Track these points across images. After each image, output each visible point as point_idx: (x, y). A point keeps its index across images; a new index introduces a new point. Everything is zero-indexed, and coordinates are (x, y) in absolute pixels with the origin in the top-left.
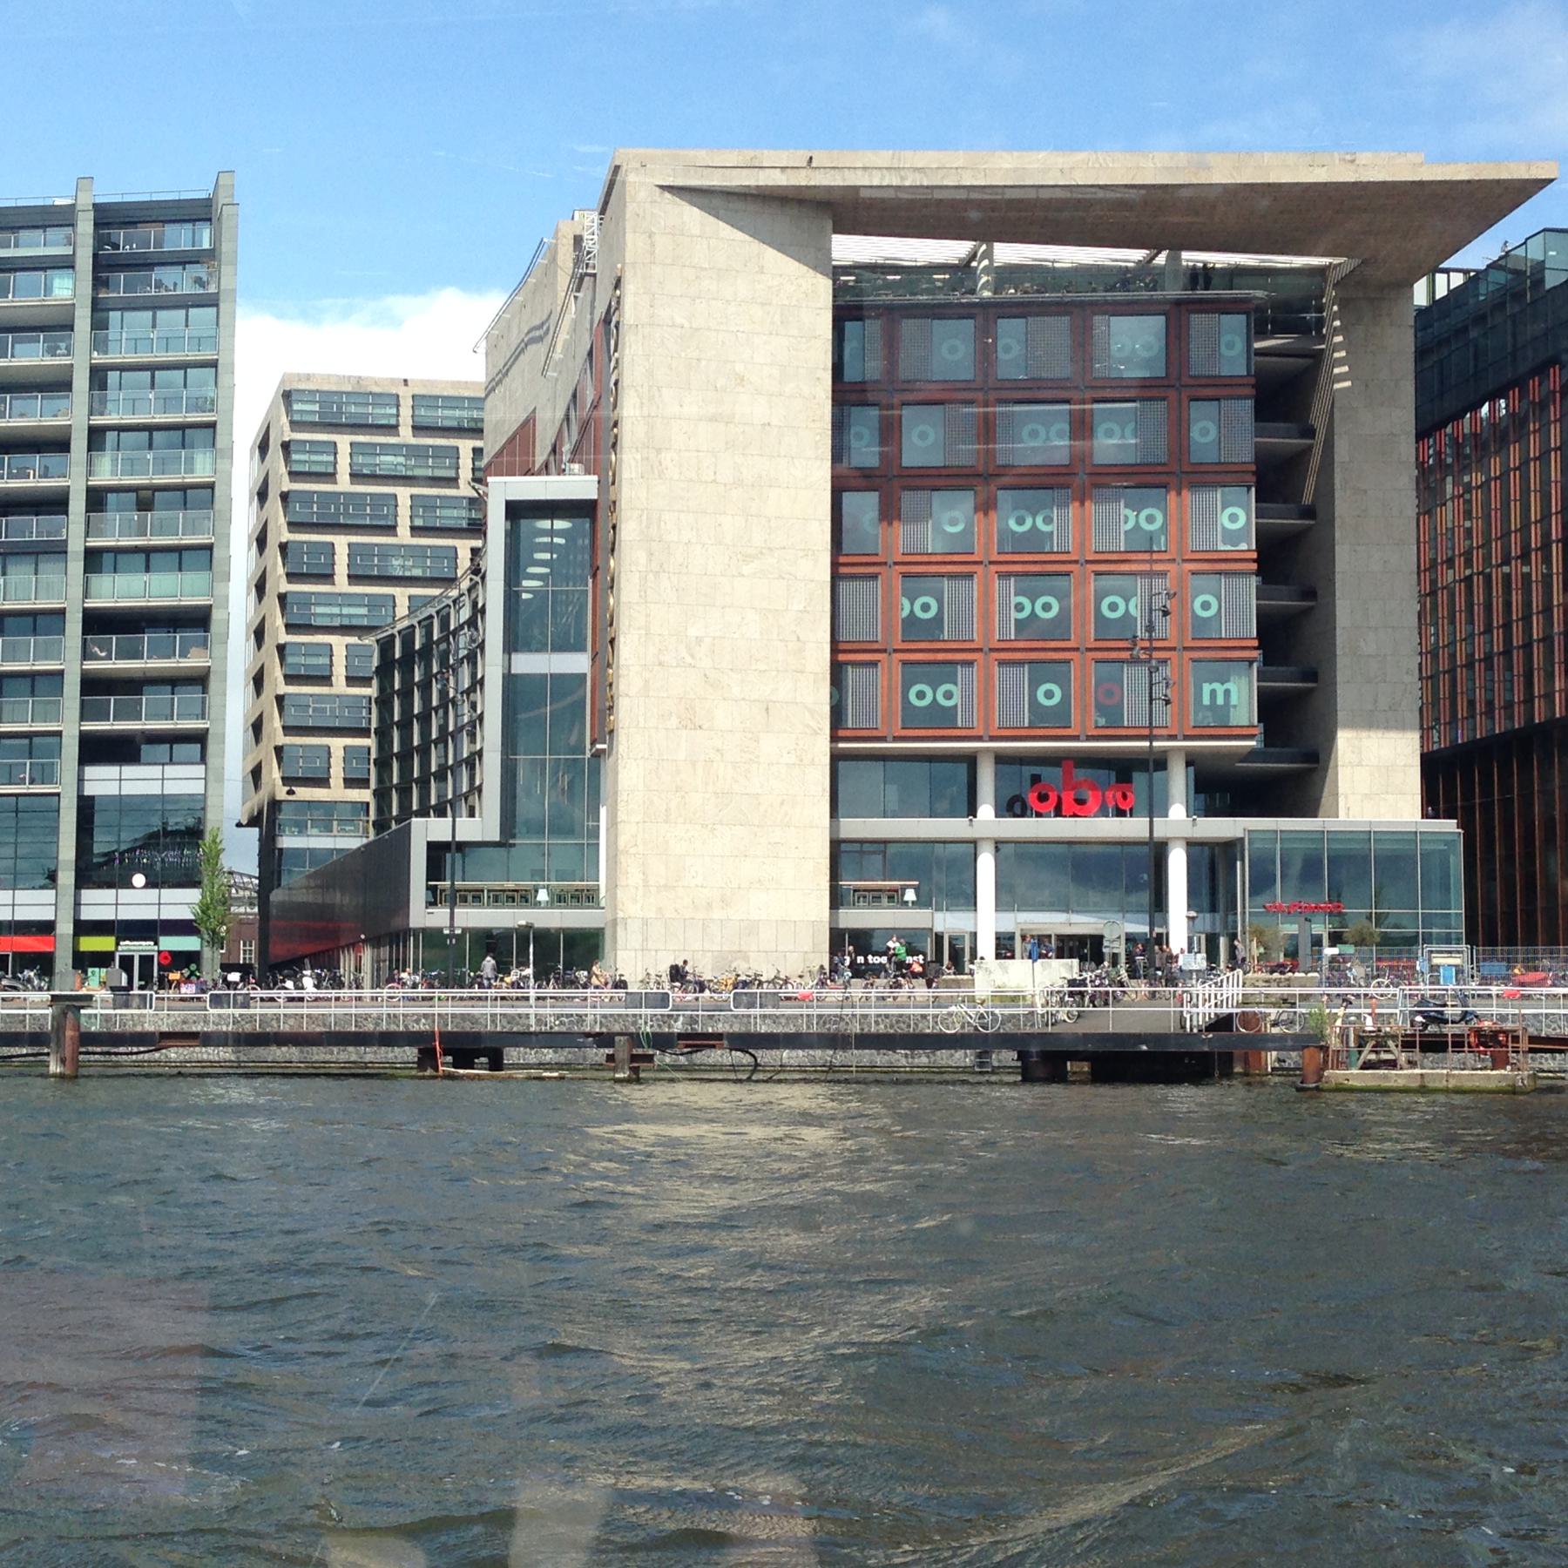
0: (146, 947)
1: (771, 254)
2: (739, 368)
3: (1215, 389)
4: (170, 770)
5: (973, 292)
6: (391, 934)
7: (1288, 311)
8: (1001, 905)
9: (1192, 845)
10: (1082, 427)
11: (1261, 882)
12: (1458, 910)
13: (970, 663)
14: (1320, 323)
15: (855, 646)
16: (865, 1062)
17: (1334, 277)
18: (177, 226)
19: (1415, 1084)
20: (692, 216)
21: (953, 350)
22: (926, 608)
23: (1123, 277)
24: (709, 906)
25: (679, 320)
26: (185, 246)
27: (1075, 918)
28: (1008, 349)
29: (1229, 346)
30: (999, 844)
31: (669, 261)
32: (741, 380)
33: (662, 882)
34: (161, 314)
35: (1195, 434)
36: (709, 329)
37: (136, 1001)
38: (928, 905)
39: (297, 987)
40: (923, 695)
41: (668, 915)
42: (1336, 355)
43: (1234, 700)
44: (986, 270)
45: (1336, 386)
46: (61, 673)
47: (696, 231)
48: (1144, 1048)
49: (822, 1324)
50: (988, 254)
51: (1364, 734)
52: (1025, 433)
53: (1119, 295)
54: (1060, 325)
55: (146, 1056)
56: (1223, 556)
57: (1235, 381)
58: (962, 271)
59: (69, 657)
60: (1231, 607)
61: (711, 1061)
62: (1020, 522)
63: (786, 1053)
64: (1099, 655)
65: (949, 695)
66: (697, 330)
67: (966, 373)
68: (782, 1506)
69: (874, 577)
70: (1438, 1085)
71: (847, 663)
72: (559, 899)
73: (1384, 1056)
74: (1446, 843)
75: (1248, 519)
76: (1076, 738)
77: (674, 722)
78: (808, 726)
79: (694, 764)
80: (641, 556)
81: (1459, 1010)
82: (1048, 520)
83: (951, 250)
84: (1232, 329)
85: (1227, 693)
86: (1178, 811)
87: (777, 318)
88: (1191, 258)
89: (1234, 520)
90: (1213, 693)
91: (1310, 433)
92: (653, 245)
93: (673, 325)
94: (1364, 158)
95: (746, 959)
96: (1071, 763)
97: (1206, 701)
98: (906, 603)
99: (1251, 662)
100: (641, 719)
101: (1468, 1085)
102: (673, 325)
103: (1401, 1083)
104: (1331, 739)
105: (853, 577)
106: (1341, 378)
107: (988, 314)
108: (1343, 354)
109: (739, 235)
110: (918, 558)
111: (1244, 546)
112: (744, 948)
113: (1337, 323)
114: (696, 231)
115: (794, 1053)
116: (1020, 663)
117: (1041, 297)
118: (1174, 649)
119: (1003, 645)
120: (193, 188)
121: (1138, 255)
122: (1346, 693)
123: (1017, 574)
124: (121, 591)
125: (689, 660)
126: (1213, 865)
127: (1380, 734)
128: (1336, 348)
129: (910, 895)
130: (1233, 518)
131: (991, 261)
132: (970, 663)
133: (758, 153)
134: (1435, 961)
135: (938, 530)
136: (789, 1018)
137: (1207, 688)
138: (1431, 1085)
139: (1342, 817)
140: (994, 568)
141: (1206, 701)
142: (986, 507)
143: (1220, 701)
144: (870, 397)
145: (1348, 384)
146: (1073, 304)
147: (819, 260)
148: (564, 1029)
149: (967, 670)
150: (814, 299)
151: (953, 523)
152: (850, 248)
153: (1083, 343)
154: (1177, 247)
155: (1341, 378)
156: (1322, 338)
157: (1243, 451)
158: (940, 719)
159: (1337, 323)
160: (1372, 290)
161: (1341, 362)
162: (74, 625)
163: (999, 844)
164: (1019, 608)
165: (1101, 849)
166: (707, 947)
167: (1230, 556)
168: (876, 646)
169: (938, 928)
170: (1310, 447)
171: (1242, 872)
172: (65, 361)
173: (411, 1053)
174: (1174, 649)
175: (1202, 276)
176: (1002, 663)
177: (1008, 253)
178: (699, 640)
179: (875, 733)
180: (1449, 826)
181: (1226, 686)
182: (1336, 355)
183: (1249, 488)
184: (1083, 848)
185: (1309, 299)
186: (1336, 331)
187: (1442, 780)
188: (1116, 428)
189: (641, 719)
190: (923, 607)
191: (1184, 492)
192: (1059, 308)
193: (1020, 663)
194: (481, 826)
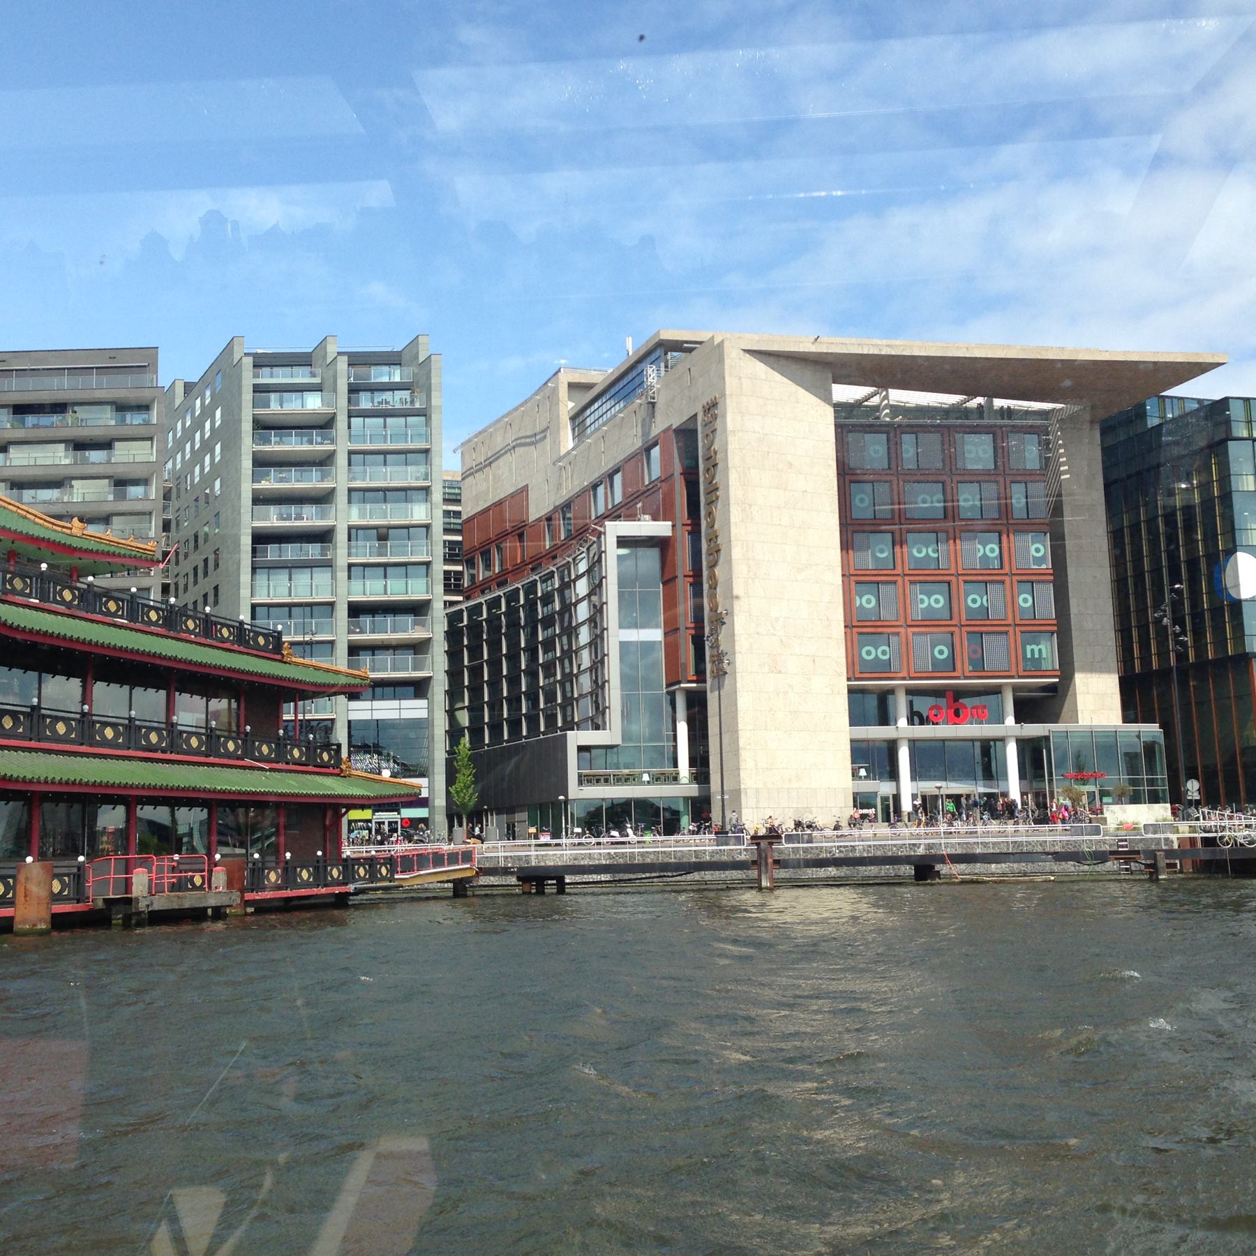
0: (392, 816)
1: (802, 391)
4: (377, 704)
6: (541, 805)
8: (915, 776)
9: (913, 743)
18: (379, 368)
20: (760, 368)
26: (385, 379)
28: (907, 452)
30: (913, 743)
32: (790, 465)
34: (389, 420)
37: (733, 841)
39: (622, 836)
43: (1044, 655)
46: (332, 643)
47: (763, 377)
51: (1089, 675)
52: (919, 499)
54: (934, 439)
55: (679, 878)
59: (341, 631)
62: (919, 551)
63: (993, 866)
64: (969, 629)
72: (656, 779)
85: (1040, 650)
90: (1032, 650)
95: (811, 812)
97: (1029, 656)
99: (1052, 633)
106: (1065, 472)
107: (892, 432)
109: (785, 380)
111: (1044, 566)
114: (763, 377)
117: (918, 421)
120: (397, 344)
124: (372, 590)
128: (1061, 456)
129: (646, 778)
130: (1037, 550)
135: (874, 556)
136: (994, 844)
137: (1029, 648)
139: (1080, 723)
141: (1029, 656)
142: (898, 541)
143: (1037, 656)
147: (826, 397)
148: (842, 855)
150: (823, 422)
151: (882, 551)
152: (846, 393)
154: (991, 395)
155: (1065, 472)
161: (1064, 464)
162: (342, 612)
165: (928, 744)
172: (331, 447)
173: (908, 870)
177: (899, 396)
178: (777, 619)
180: (1152, 730)
187: (1135, 701)
188: (928, 498)
193: (926, 634)
194: (610, 736)
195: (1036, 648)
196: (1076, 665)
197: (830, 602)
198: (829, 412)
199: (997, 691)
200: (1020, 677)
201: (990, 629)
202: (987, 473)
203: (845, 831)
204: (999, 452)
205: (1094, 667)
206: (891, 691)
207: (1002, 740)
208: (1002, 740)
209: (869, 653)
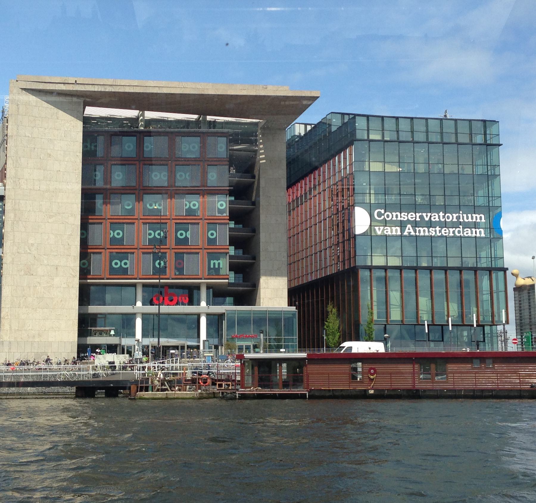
1: (61, 113)
2: (49, 151)
3: (216, 162)
5: (137, 127)
7: (247, 136)
10: (172, 175)
11: (231, 326)
12: (296, 337)
13: (133, 253)
14: (256, 141)
15: (94, 247)
16: (56, 391)
17: (260, 126)
19: (164, 397)
20: (32, 99)
21: (129, 147)
22: (118, 234)
23: (187, 123)
25: (27, 135)
27: (170, 340)
29: (221, 147)
30: (208, 315)
31: (24, 114)
32: (50, 155)
33: (17, 328)
35: (209, 177)
36: (38, 138)
38: (120, 336)
40: (117, 264)
41: (19, 340)
42: (261, 151)
43: (221, 266)
44: (142, 120)
45: (261, 162)
48: (112, 385)
50: (143, 115)
51: (269, 278)
53: (185, 130)
56: (218, 218)
57: (222, 160)
58: (135, 120)
60: (222, 235)
61: (4, 392)
63: (29, 388)
65: (126, 264)
66: (34, 138)
69: (101, 223)
70: (171, 397)
71: (91, 253)
73: (163, 387)
74: (293, 314)
75: (226, 205)
76: (168, 279)
77: (23, 273)
78: (71, 274)
79: (29, 287)
81: (207, 371)
82: (160, 205)
83: (132, 113)
84: (222, 141)
85: (219, 264)
86: (203, 304)
87: (63, 135)
88: (209, 118)
89: (222, 204)
90: (214, 264)
91: (254, 177)
92: (18, 108)
93: (25, 136)
94: (270, 87)
97: (212, 266)
98: (112, 232)
100: (11, 272)
101: (180, 396)
102: (25, 136)
103: (160, 396)
104: (259, 280)
105: (94, 223)
106: (263, 159)
108: (263, 151)
110: (212, 218)
111: (225, 215)
112: (46, 351)
113: (261, 141)
115: (32, 388)
116: (150, 253)
118: (201, 249)
119: (144, 247)
121: (195, 117)
122: (264, 264)
123: (149, 223)
125: (29, 251)
126: (216, 321)
127: (274, 278)
128: (261, 149)
129: (112, 332)
131: (144, 117)
132: (133, 253)
133: (67, 78)
134: (205, 355)
135: (123, 207)
137: (212, 262)
138: (169, 397)
140: (141, 221)
141: (212, 266)
142: (139, 199)
143: (217, 266)
144: (153, 162)
145: (264, 161)
146: (167, 132)
149: (132, 255)
151: (129, 205)
152: (91, 111)
153: (172, 146)
154: (203, 113)
155: (263, 159)
156: (257, 146)
157: (225, 184)
158: (124, 272)
159: (261, 141)
160: (273, 130)
161: (262, 154)
163: (208, 315)
164: (150, 234)
166: (33, 351)
167: (220, 218)
168: (101, 247)
169: (123, 344)
170: (254, 182)
171: (225, 323)
174: (201, 249)
175: (213, 124)
176: (143, 253)
177: (150, 115)
178: (32, 245)
179: (198, 277)
180: (293, 308)
181: (219, 261)
182: (261, 151)
183: (227, 195)
184: (173, 316)
185: (253, 133)
186: (261, 144)
187: (294, 294)
189: (11, 272)
190: (117, 234)
191: (205, 196)
192: (166, 134)
193: (150, 253)
195: (217, 262)
196: (261, 271)
197: (71, 235)
198: (80, 125)
199: (134, 285)
200: (173, 279)
201: (189, 251)
202: (195, 160)
203: (70, 366)
204: (140, 145)
205: (272, 273)
206: (198, 287)
207: (135, 314)
209: (116, 264)
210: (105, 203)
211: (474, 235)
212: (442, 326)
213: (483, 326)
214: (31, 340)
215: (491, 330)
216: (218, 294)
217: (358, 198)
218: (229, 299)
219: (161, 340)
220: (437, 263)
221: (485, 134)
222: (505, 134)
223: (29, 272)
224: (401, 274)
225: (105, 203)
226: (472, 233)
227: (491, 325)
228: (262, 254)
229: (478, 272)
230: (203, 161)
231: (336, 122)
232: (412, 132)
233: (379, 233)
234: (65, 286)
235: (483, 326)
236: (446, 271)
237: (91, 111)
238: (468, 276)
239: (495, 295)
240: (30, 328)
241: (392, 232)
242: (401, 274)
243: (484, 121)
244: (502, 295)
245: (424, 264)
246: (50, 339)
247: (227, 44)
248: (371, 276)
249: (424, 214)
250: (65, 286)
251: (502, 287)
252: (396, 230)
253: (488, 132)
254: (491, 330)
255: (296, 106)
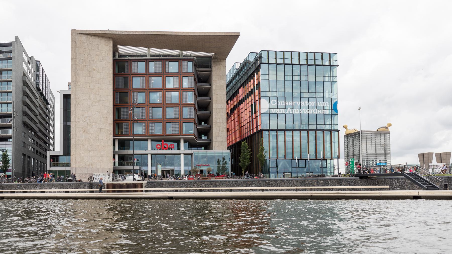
2: (94, 67)
3: (187, 75)
24: (89, 165)
47: (85, 42)
49: (162, 221)
67: (144, 71)
68: (195, 221)
77: (81, 132)
79: (86, 140)
80: (75, 101)
84: (190, 64)
96: (163, 141)
146: (161, 59)
153: (164, 67)
178: (86, 117)
180: (229, 151)
204: (147, 67)
208: (180, 154)
210: (431, 163)
211: (323, 113)
212: (305, 160)
213: (326, 160)
214: (87, 167)
215: (331, 162)
216: (192, 145)
217: (262, 94)
218: (203, 148)
219: (135, 167)
220: (304, 127)
221: (330, 60)
222: (338, 60)
223: (85, 132)
224: (285, 133)
225: (431, 163)
226: (322, 112)
227: (330, 159)
228: (214, 124)
229: (325, 132)
230: (147, 75)
231: (254, 57)
232: (292, 59)
233: (274, 112)
234: (105, 139)
235: (326, 160)
236: (323, 132)
237: (123, 49)
238: (320, 134)
239: (333, 144)
240: (87, 161)
241: (280, 111)
242: (285, 133)
243: (330, 54)
244: (337, 144)
245: (297, 128)
246: (98, 167)
247: (360, 109)
248: (269, 135)
249: (297, 102)
250: (105, 139)
251: (337, 140)
252: (282, 111)
253: (331, 59)
254: (331, 162)
255: (232, 39)
